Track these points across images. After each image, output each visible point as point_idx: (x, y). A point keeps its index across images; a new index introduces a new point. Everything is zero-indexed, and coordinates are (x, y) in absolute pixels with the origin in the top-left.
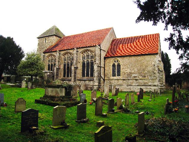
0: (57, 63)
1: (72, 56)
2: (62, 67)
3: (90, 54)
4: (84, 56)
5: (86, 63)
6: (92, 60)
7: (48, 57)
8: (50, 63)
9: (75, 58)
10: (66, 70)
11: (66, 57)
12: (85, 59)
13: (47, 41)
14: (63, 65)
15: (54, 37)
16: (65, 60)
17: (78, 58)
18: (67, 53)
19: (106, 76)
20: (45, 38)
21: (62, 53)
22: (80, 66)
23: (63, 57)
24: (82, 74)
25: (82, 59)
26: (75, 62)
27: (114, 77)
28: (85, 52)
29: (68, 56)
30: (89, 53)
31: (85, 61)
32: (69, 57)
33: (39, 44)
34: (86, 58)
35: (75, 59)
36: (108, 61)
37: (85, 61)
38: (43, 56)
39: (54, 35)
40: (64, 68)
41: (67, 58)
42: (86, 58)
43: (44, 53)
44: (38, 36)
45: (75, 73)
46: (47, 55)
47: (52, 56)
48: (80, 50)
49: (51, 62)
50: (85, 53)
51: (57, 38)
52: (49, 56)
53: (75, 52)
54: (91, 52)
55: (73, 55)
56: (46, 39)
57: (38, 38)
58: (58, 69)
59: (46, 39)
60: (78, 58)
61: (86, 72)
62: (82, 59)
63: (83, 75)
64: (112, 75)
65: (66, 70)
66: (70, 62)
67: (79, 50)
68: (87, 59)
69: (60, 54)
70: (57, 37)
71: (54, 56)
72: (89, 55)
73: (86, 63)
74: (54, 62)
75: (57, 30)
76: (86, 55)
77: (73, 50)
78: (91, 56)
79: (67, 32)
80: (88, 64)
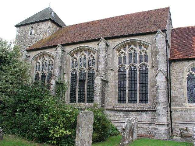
0: (57, 71)
1: (92, 56)
2: (67, 79)
3: (87, 57)
4: (122, 55)
5: (127, 71)
6: (143, 64)
7: (36, 58)
8: (39, 72)
9: (102, 60)
10: (78, 87)
11: (78, 58)
12: (125, 63)
13: (33, 32)
14: (70, 76)
15: (50, 23)
16: (74, 64)
17: (108, 60)
18: (81, 50)
19: (173, 102)
20: (30, 26)
21: (69, 49)
22: (113, 78)
23: (71, 58)
24: (117, 96)
25: (117, 63)
26: (101, 68)
27: (191, 103)
28: (76, 52)
29: (83, 57)
30: (47, 58)
31: (127, 66)
32: (85, 58)
33: (17, 36)
34: (127, 60)
35: (103, 63)
36: (176, 67)
37: (127, 66)
38: (26, 56)
39: (50, 20)
40: (72, 83)
41: (79, 60)
42: (127, 60)
43: (28, 51)
44: (16, 24)
45: (103, 93)
46: (33, 54)
47: (45, 57)
48: (114, 43)
49: (43, 70)
50: (125, 50)
51: (55, 26)
52: (39, 57)
53: (102, 44)
54: (140, 48)
55: (53, 58)
56: (32, 27)
57: (17, 26)
58: (60, 84)
59: (32, 27)
60: (108, 60)
61: (127, 92)
62: (117, 61)
63: (121, 99)
64: (187, 102)
65: (78, 87)
66: (86, 70)
67: (109, 42)
68: (130, 62)
69: (63, 51)
70: (54, 25)
71: (49, 56)
72: (135, 54)
73: (127, 71)
74: (49, 69)
75: (47, 17)
76: (127, 53)
77: (96, 43)
78: (141, 56)
79: (69, 19)
80: (133, 73)
